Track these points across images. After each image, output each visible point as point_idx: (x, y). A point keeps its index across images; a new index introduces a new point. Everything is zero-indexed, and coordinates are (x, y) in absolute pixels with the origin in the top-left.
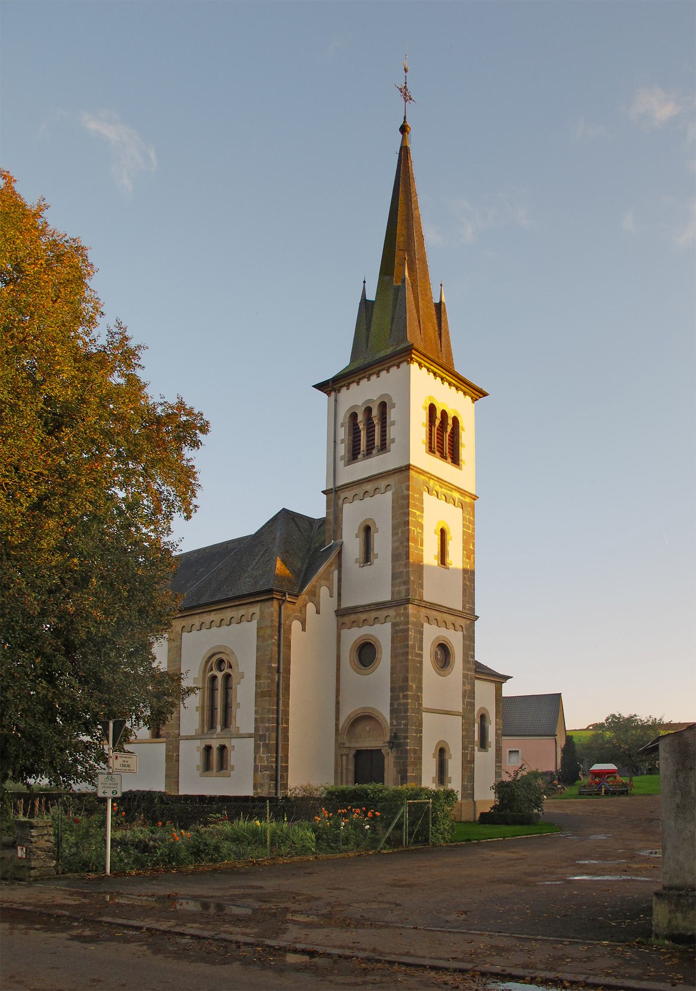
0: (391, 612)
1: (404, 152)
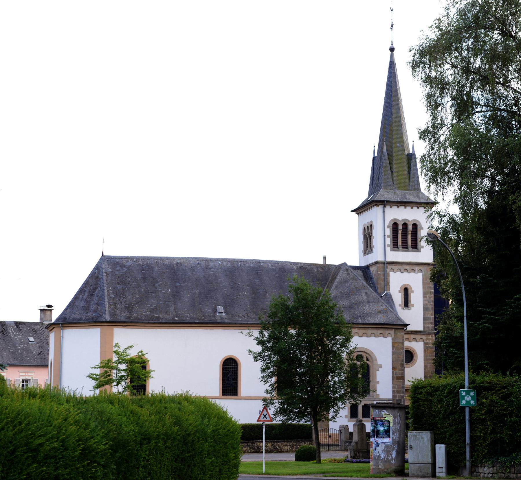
0: (424, 337)
1: (392, 65)
